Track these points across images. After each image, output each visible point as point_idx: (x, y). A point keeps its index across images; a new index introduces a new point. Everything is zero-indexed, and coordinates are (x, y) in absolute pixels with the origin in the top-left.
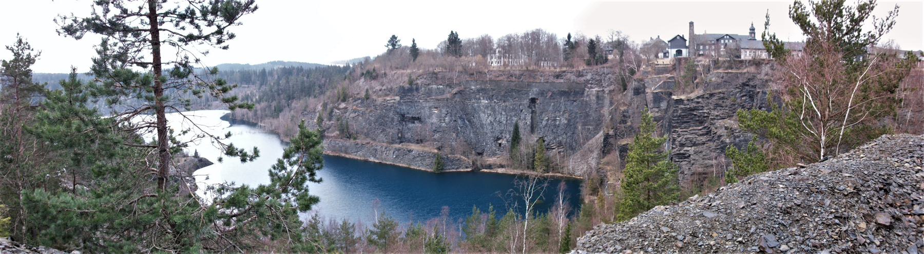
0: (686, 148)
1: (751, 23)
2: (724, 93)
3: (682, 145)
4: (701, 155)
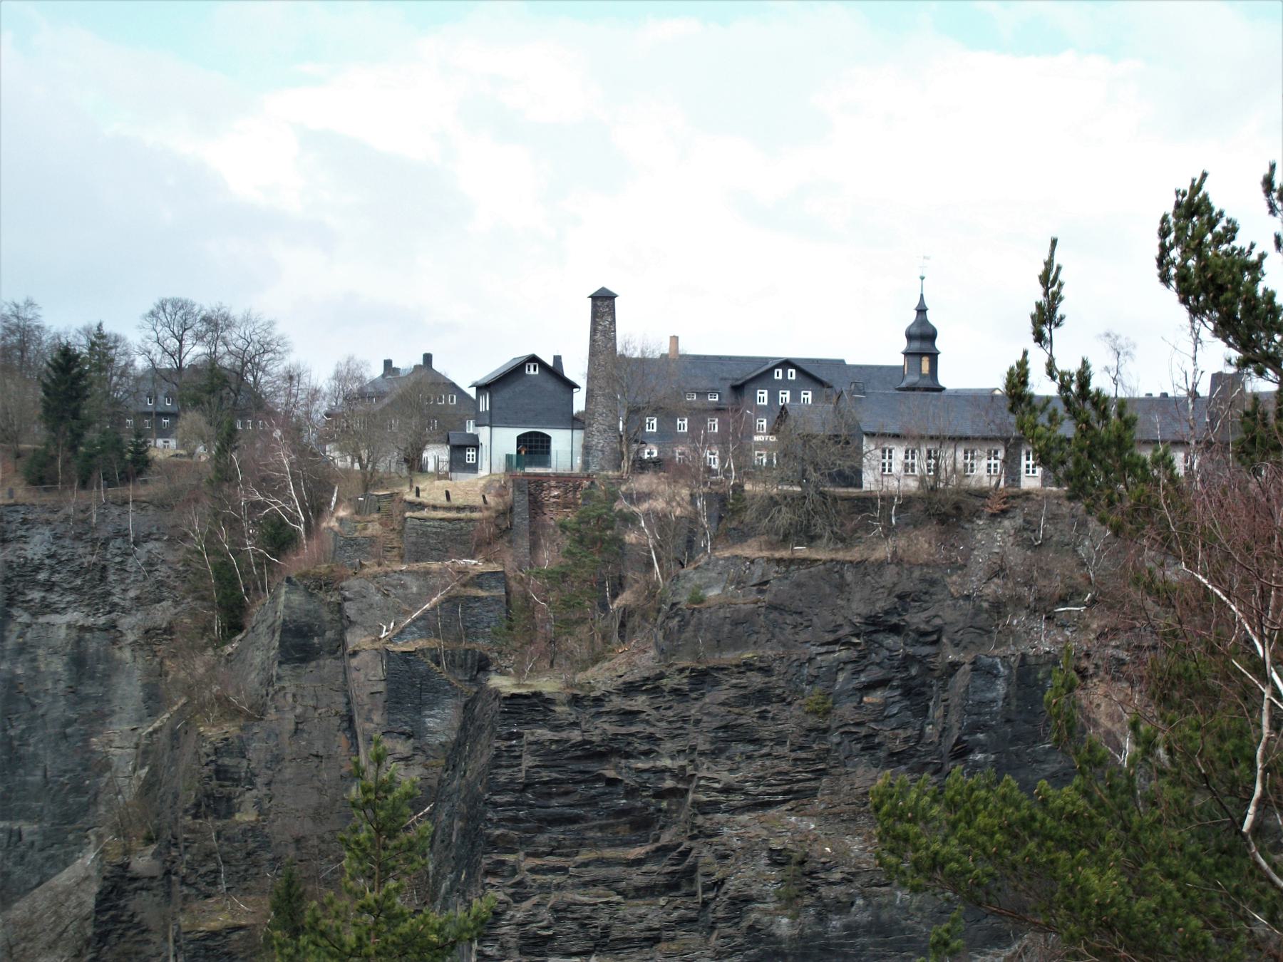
2: (766, 671)
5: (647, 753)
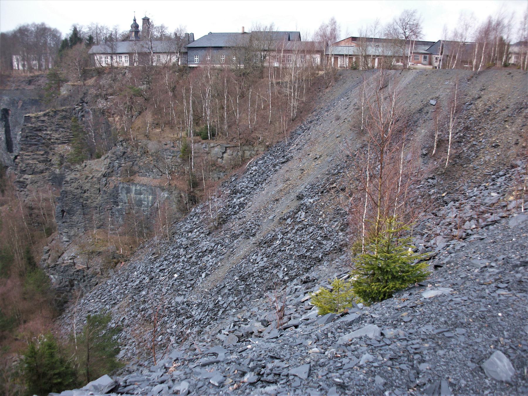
0: (26, 176)
1: (133, 18)
2: (66, 111)
3: (23, 172)
4: (36, 186)
5: (46, 130)
